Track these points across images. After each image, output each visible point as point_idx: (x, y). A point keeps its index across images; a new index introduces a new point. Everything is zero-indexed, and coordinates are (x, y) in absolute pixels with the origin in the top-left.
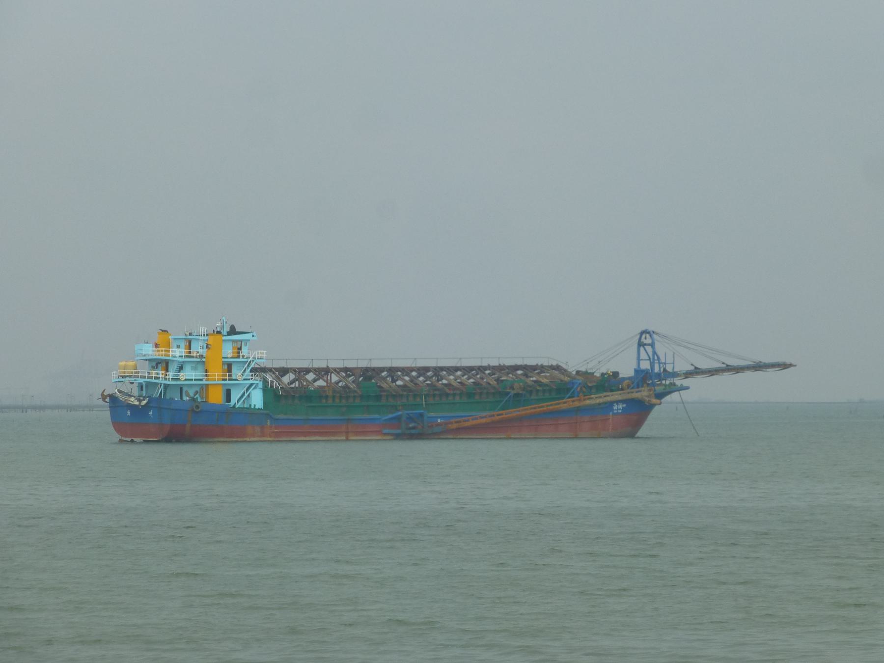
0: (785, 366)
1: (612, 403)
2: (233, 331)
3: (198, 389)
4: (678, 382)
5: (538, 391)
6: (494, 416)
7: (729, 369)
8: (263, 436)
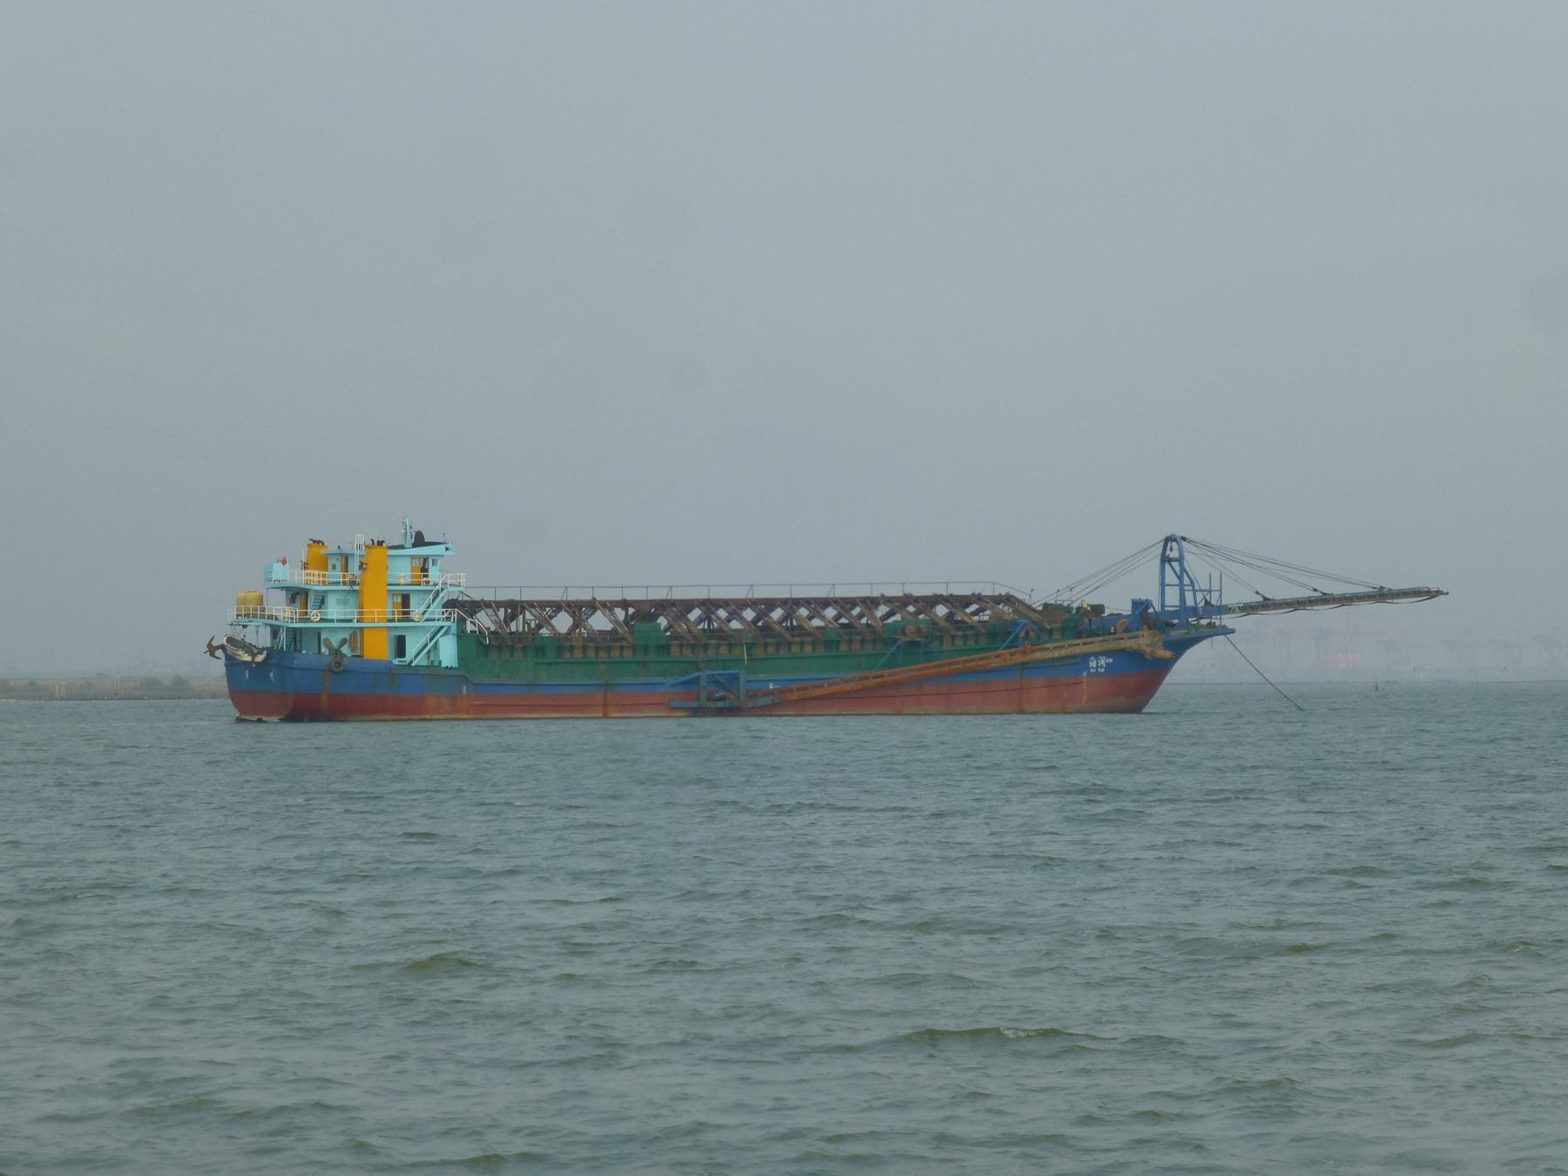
0: (1431, 594)
1: (1086, 657)
2: (419, 541)
3: (346, 635)
4: (1227, 621)
5: (953, 637)
6: (867, 678)
7: (1326, 599)
8: (454, 711)
